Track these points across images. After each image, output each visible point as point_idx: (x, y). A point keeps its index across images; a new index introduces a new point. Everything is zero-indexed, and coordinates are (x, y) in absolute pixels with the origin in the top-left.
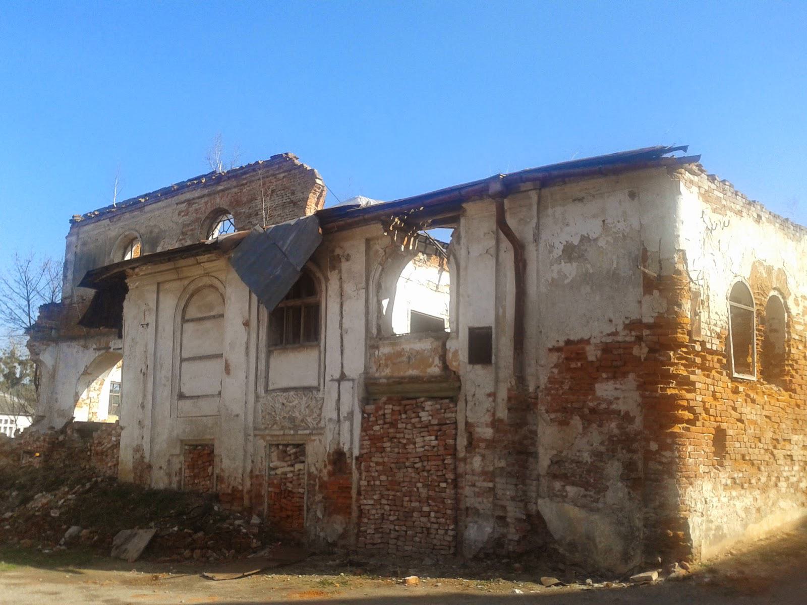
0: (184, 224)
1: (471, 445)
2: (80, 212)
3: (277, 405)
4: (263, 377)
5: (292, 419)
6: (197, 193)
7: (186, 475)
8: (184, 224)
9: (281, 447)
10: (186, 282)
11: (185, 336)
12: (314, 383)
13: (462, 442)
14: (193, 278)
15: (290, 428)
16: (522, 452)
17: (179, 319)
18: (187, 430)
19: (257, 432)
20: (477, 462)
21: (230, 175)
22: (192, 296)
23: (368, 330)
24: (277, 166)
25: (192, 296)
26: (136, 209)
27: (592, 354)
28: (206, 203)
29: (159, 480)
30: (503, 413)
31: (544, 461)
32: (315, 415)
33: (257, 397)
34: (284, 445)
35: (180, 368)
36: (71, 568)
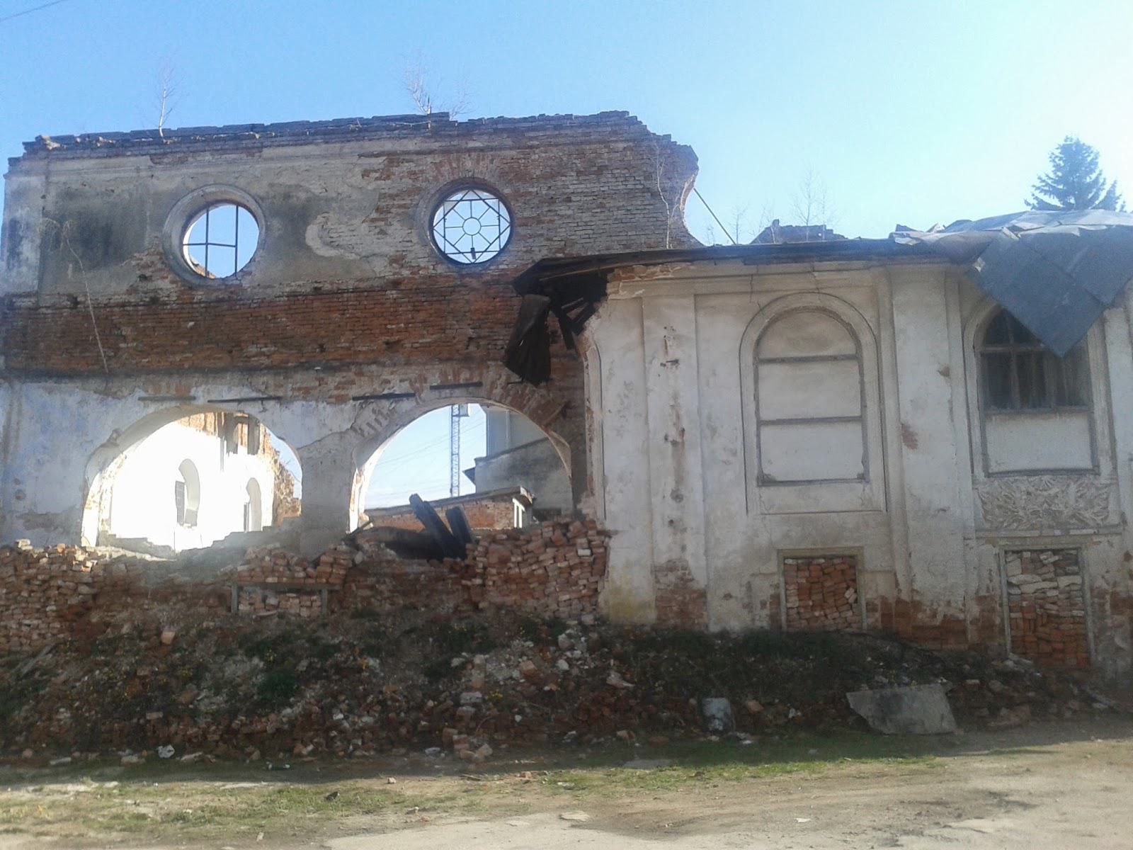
0: (380, 195)
2: (51, 128)
3: (1018, 495)
4: (980, 454)
5: (1054, 515)
6: (411, 145)
7: (789, 605)
8: (380, 195)
9: (1027, 555)
10: (764, 300)
11: (762, 386)
12: (1086, 463)
14: (781, 294)
17: (749, 358)
18: (793, 534)
19: (981, 534)
21: (500, 126)
22: (774, 321)
24: (609, 129)
25: (774, 321)
26: (236, 149)
28: (438, 166)
29: (728, 616)
34: (1033, 551)
35: (758, 436)
36: (863, 760)
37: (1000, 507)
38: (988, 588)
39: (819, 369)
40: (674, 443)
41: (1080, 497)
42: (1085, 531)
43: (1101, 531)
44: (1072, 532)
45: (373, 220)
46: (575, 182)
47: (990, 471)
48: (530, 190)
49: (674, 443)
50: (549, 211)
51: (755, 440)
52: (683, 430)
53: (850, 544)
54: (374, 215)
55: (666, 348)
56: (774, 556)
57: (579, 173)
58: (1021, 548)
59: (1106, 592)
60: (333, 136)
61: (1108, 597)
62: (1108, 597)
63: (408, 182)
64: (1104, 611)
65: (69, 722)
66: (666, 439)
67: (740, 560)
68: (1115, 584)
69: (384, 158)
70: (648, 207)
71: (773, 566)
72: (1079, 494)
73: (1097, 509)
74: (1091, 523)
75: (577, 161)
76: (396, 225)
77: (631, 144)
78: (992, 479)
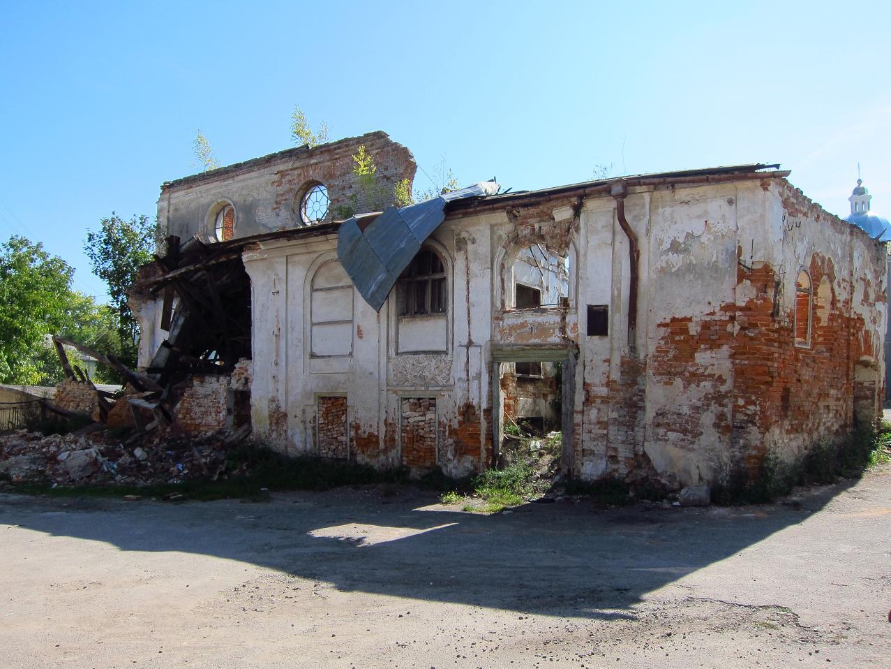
1: (588, 401)
5: (423, 378)
10: (314, 256)
11: (313, 302)
13: (579, 397)
15: (421, 385)
16: (633, 406)
20: (593, 414)
21: (323, 149)
22: (320, 267)
23: (492, 303)
27: (694, 329)
30: (616, 375)
31: (649, 415)
33: (388, 358)
35: (311, 331)
37: (400, 372)
39: (337, 294)
40: (276, 336)
42: (436, 388)
43: (444, 389)
44: (430, 389)
45: (275, 209)
49: (276, 336)
53: (342, 391)
54: (275, 206)
58: (408, 397)
59: (446, 425)
61: (447, 428)
62: (447, 428)
64: (445, 436)
65: (559, 443)
68: (450, 421)
71: (312, 401)
74: (441, 384)
76: (283, 210)
77: (379, 150)
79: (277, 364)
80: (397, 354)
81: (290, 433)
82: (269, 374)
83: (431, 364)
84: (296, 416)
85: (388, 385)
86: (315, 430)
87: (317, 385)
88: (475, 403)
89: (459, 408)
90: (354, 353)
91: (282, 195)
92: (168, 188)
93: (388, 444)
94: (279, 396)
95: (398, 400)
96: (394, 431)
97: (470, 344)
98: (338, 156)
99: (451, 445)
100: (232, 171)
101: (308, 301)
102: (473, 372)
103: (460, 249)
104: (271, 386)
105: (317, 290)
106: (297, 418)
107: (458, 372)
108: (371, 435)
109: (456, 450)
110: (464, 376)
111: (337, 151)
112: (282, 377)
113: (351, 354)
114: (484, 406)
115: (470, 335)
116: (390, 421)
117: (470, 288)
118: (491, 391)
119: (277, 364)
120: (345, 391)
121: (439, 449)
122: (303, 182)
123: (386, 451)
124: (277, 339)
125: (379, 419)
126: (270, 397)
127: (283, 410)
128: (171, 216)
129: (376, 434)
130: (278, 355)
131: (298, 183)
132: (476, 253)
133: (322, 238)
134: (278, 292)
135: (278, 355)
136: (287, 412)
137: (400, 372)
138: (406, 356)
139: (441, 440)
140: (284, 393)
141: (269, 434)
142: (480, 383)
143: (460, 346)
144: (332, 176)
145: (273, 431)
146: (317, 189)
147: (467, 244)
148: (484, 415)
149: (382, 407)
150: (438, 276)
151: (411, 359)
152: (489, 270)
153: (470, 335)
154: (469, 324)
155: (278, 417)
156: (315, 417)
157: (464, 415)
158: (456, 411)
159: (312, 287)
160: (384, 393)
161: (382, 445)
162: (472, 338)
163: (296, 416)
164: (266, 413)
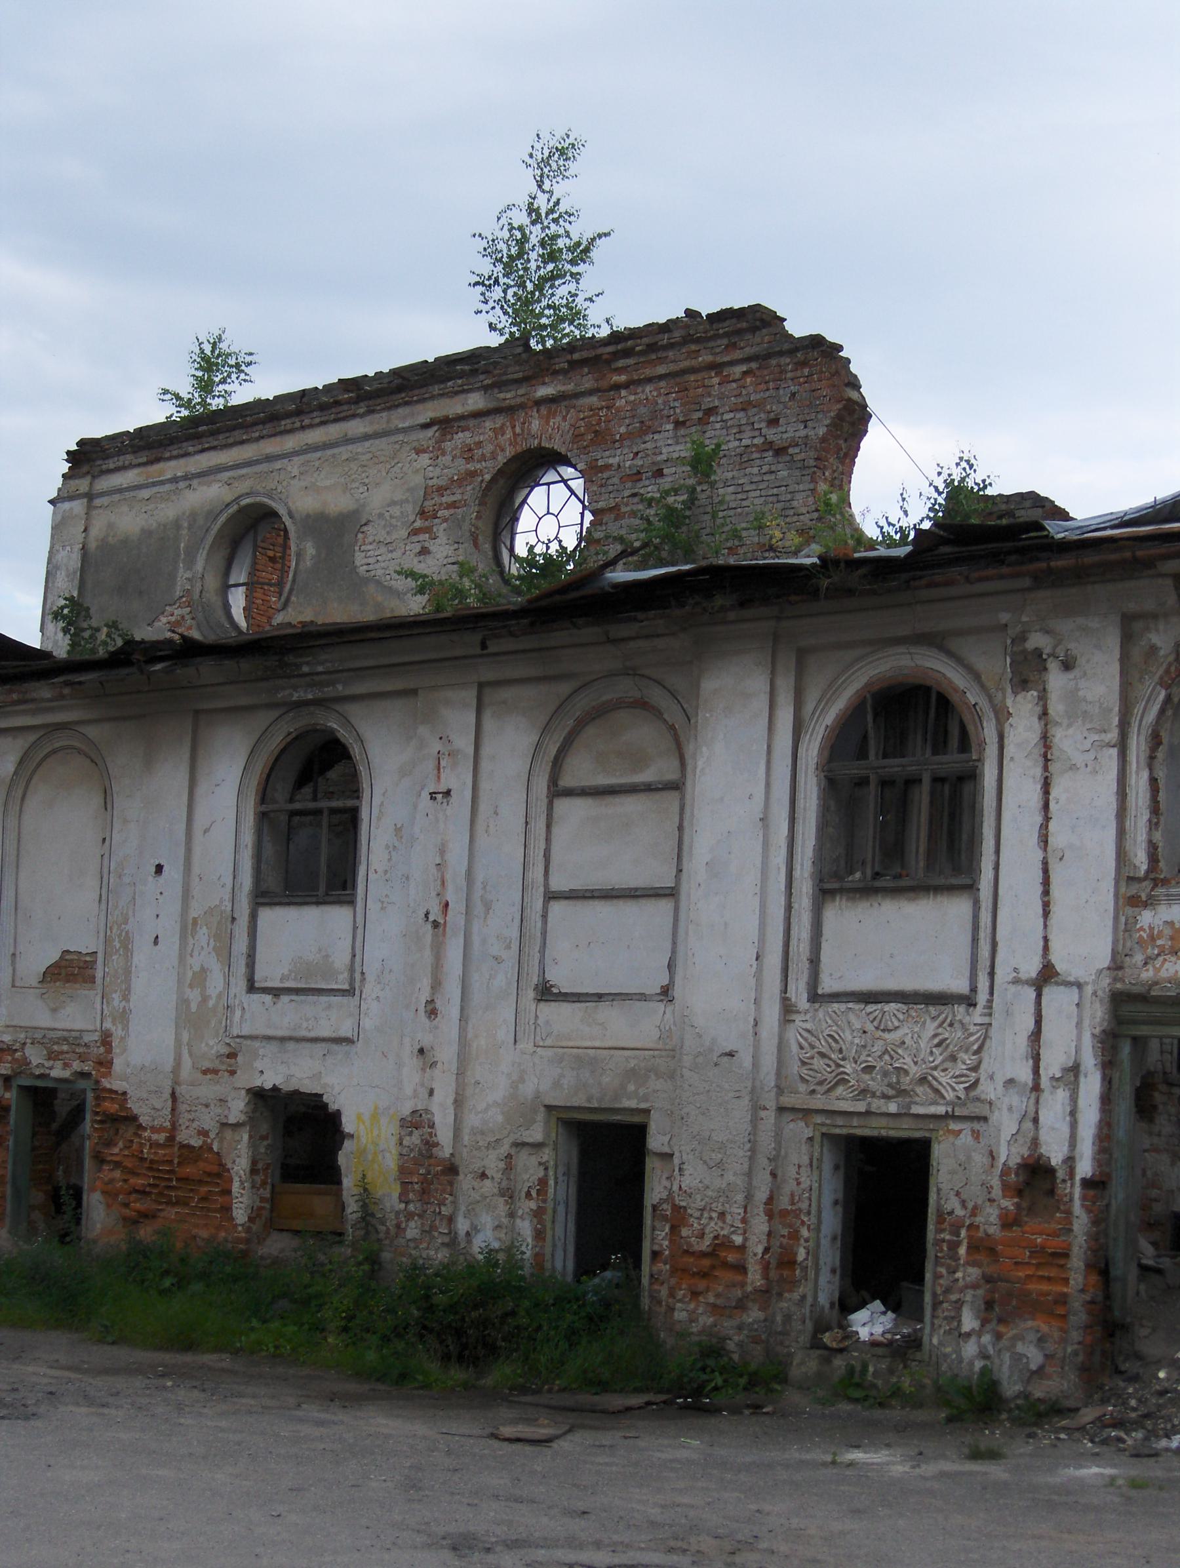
11: (555, 830)
12: (960, 985)
17: (541, 785)
21: (576, 356)
23: (1122, 856)
32: (960, 1068)
33: (788, 1009)
35: (545, 917)
38: (792, 1195)
39: (630, 805)
40: (436, 924)
41: (938, 1045)
46: (670, 442)
47: (820, 992)
48: (611, 461)
49: (436, 924)
50: (634, 495)
51: (539, 924)
52: (447, 905)
53: (633, 1104)
54: (418, 524)
55: (439, 769)
56: (541, 1116)
57: (678, 424)
60: (379, 401)
62: (963, 1233)
63: (462, 466)
66: (427, 915)
67: (500, 1118)
68: (974, 1212)
69: (436, 428)
70: (765, 478)
72: (936, 1041)
73: (960, 1068)
74: (950, 1095)
75: (677, 404)
76: (442, 539)
77: (754, 365)
78: (817, 1005)
79: (432, 1012)
80: (815, 997)
81: (462, 1225)
82: (407, 1040)
83: (916, 1035)
84: (483, 1176)
85: (780, 1090)
86: (541, 1221)
87: (557, 1084)
88: (1056, 1159)
89: (1006, 1171)
90: (677, 992)
91: (441, 490)
92: (87, 457)
93: (773, 1274)
94: (435, 1109)
95: (811, 1139)
96: (795, 1236)
97: (1047, 975)
98: (623, 378)
99: (975, 1286)
100: (288, 415)
101: (539, 826)
102: (1054, 1062)
103: (1022, 684)
104: (411, 1074)
105: (569, 793)
106: (487, 1182)
107: (1007, 1059)
108: (722, 1243)
109: (989, 1305)
110: (1024, 1074)
111: (621, 363)
112: (447, 1054)
113: (666, 993)
114: (1085, 1168)
115: (1046, 948)
116: (784, 1203)
117: (1052, 805)
118: (1109, 1125)
119: (432, 1012)
120: (643, 1106)
121: (934, 1295)
122: (509, 452)
123: (765, 1295)
124: (435, 936)
125: (749, 1197)
126: (406, 1109)
127: (446, 1151)
128: (92, 545)
129: (738, 1240)
130: (436, 985)
131: (494, 457)
132: (1072, 697)
133: (589, 633)
134: (448, 793)
135: (436, 985)
136: (457, 1161)
137: (822, 1055)
138: (843, 1007)
139: (943, 1270)
140: (450, 1100)
141: (398, 1226)
142: (1074, 1099)
143: (1016, 981)
144: (601, 437)
145: (410, 1216)
146: (550, 476)
147: (1045, 669)
148: (1084, 1198)
149: (762, 1161)
150: (950, 762)
151: (858, 1017)
152: (1114, 752)
153: (1046, 948)
154: (1046, 914)
155: (431, 1172)
156: (543, 1182)
157: (1020, 1193)
158: (996, 1182)
159: (553, 780)
160: (769, 1117)
161: (755, 1277)
162: (1055, 958)
163: (483, 1176)
164: (391, 1162)
